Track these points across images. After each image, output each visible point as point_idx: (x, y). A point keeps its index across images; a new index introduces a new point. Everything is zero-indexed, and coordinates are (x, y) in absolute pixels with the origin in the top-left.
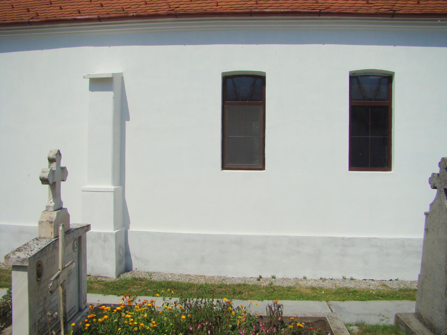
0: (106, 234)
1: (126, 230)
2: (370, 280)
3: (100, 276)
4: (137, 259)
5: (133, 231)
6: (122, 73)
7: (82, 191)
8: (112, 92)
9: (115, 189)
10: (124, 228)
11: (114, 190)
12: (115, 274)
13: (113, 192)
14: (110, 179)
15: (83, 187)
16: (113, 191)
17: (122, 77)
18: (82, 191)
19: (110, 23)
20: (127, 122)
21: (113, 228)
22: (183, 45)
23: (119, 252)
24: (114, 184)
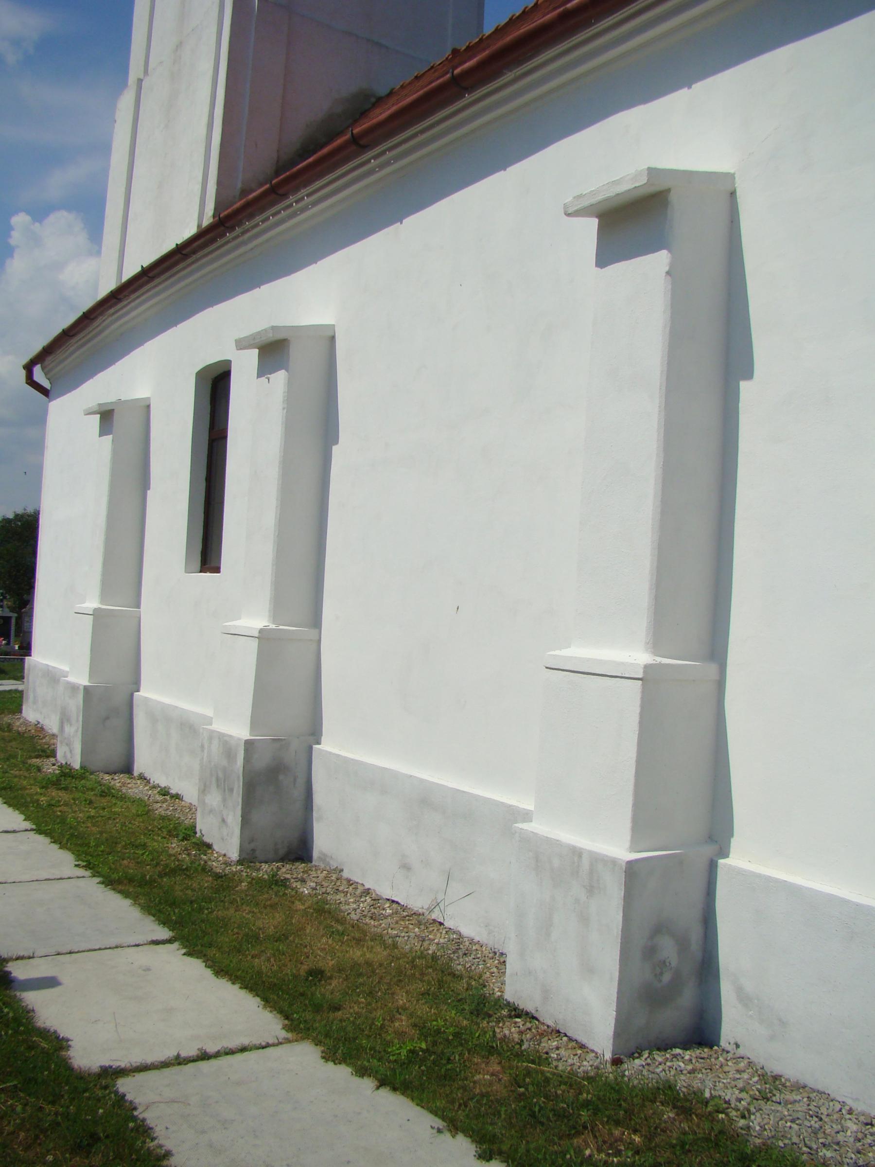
0: (597, 859)
1: (715, 859)
2: (29, 958)
3: (566, 1035)
4: (744, 998)
5: (731, 868)
6: (731, 177)
7: (547, 668)
8: (283, 372)
9: (647, 667)
10: (708, 850)
11: (644, 672)
12: (611, 1041)
13: (640, 682)
14: (642, 623)
15: (548, 653)
16: (640, 676)
17: (733, 194)
18: (547, 668)
19: (529, 67)
20: (148, 491)
21: (629, 838)
22: (501, 170)
23: (650, 952)
24: (656, 644)
